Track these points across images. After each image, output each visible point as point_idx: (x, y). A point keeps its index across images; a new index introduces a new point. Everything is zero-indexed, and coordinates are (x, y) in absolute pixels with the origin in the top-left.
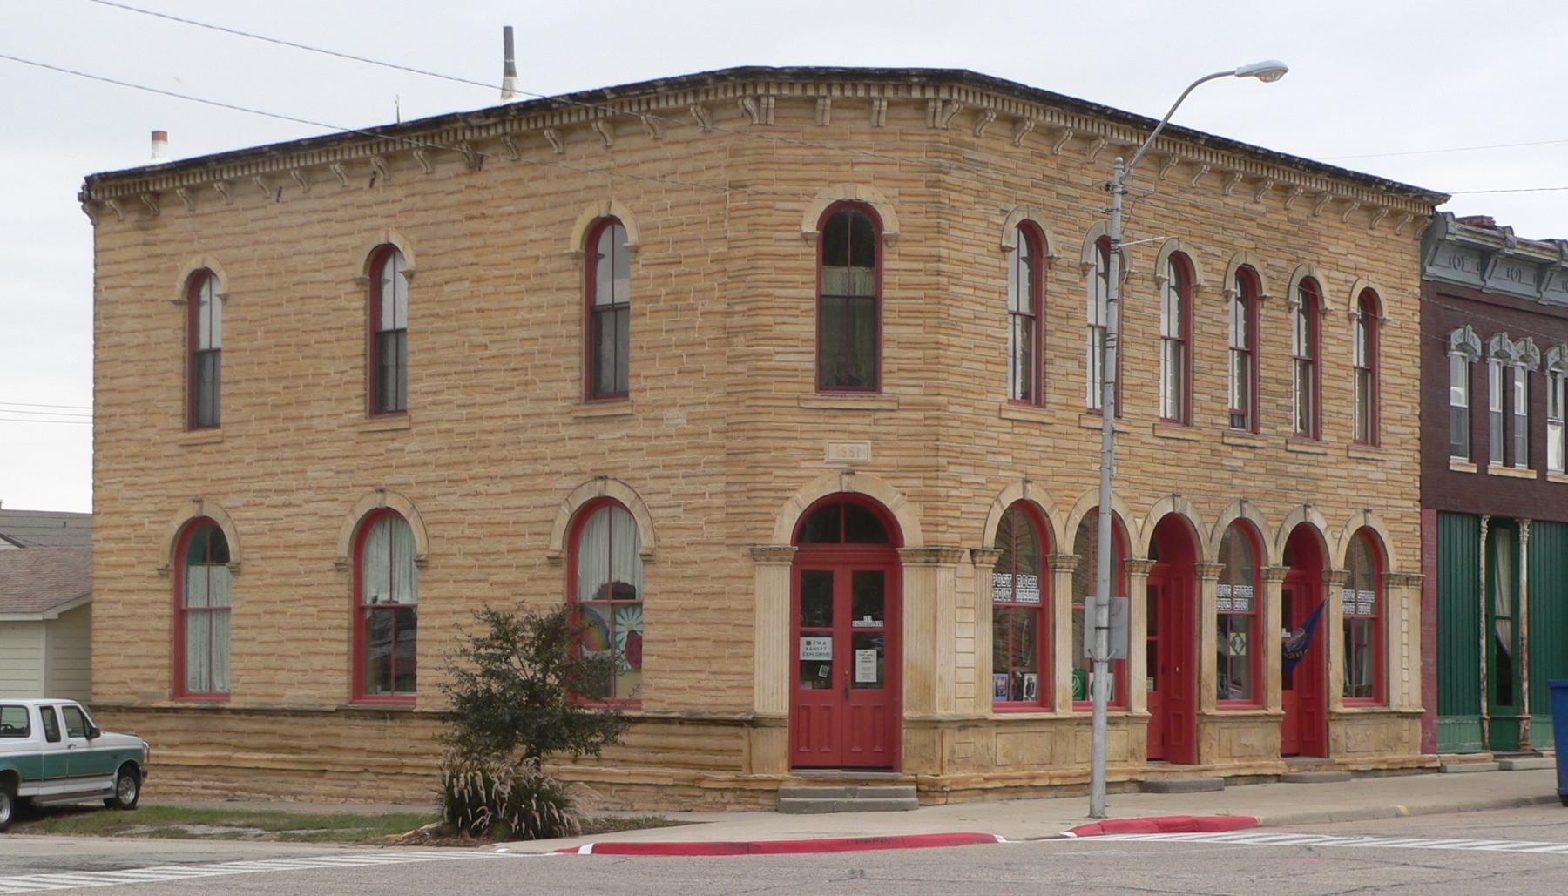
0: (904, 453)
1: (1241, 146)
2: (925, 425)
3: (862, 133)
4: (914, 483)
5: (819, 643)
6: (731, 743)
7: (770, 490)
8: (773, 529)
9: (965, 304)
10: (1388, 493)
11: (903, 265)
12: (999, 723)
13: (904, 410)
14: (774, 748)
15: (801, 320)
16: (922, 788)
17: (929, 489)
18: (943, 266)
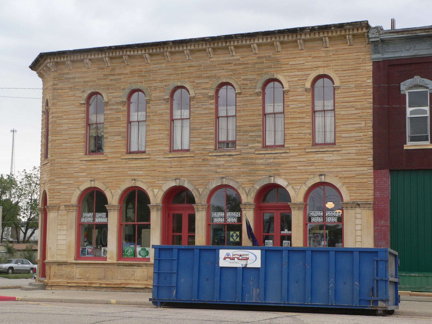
9: (63, 125)
10: (343, 165)
12: (76, 264)
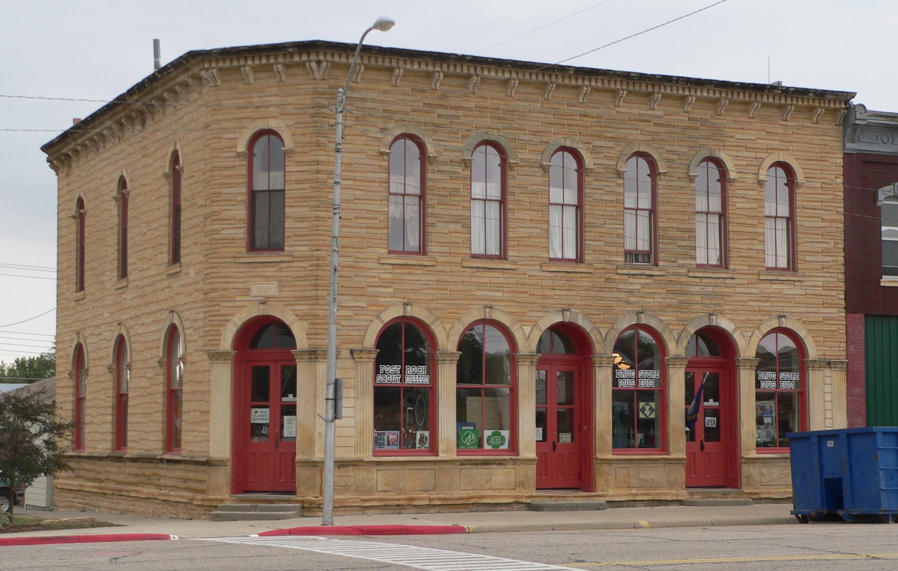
0: (297, 289)
1: (611, 73)
2: (310, 270)
3: (272, 87)
4: (303, 308)
5: (262, 412)
6: (199, 476)
7: (219, 316)
8: (220, 340)
11: (298, 168)
12: (378, 463)
13: (297, 261)
14: (222, 478)
15: (238, 207)
16: (306, 505)
17: (312, 311)
18: (320, 167)
